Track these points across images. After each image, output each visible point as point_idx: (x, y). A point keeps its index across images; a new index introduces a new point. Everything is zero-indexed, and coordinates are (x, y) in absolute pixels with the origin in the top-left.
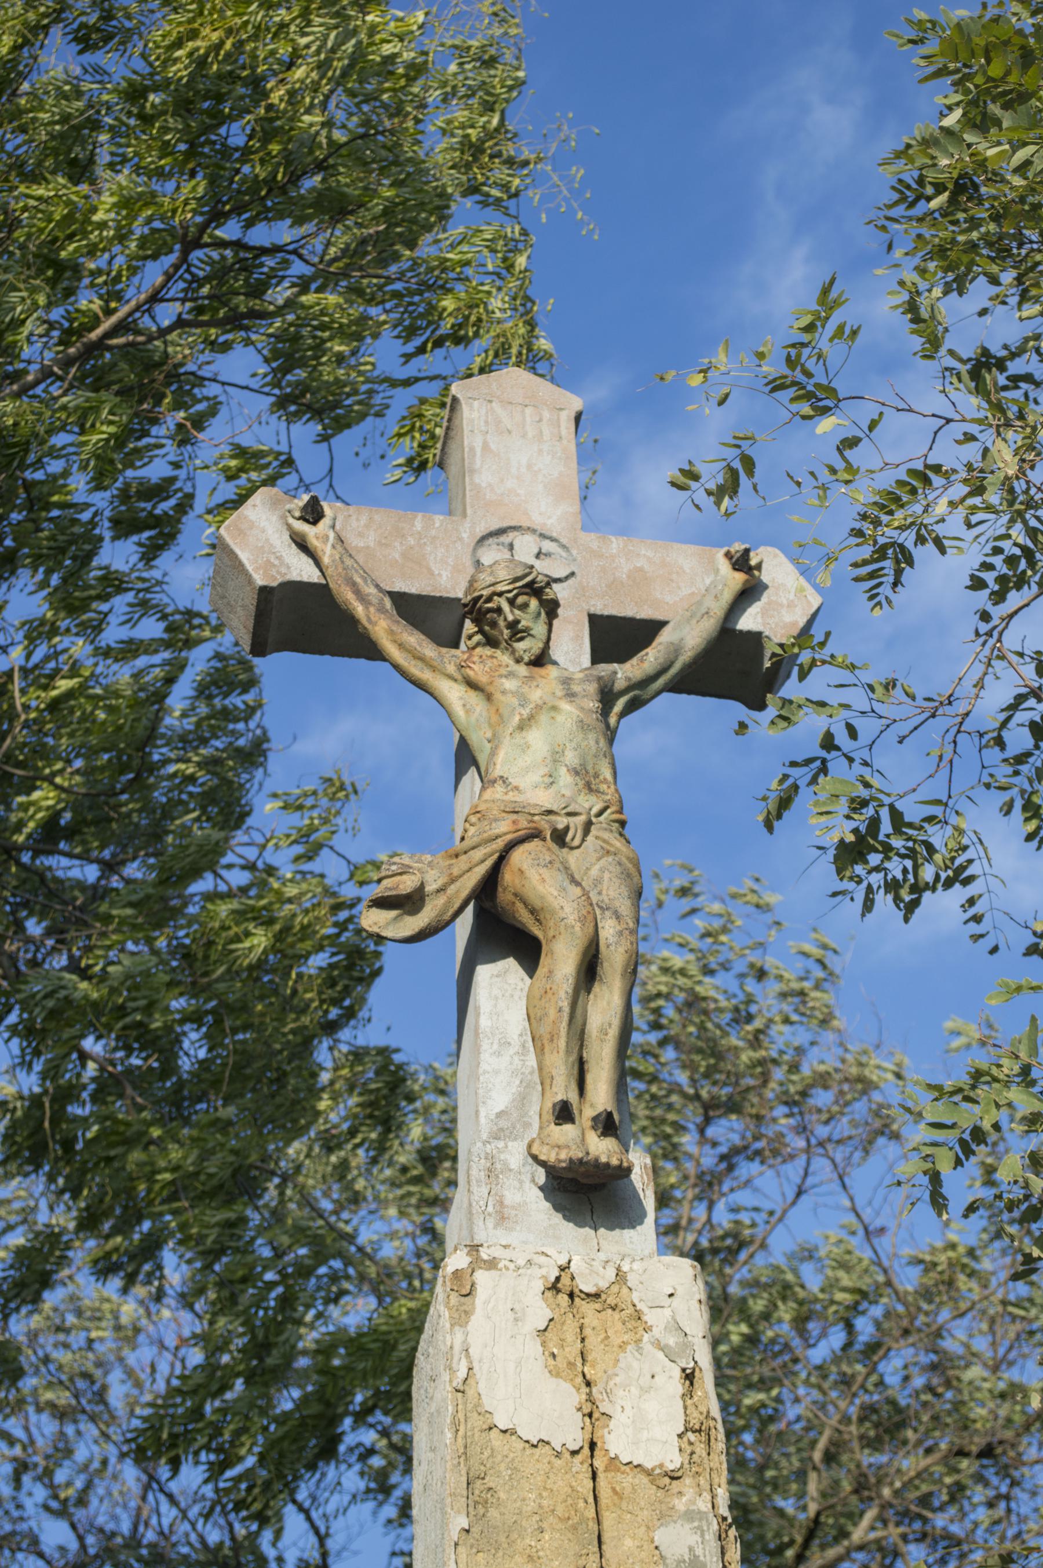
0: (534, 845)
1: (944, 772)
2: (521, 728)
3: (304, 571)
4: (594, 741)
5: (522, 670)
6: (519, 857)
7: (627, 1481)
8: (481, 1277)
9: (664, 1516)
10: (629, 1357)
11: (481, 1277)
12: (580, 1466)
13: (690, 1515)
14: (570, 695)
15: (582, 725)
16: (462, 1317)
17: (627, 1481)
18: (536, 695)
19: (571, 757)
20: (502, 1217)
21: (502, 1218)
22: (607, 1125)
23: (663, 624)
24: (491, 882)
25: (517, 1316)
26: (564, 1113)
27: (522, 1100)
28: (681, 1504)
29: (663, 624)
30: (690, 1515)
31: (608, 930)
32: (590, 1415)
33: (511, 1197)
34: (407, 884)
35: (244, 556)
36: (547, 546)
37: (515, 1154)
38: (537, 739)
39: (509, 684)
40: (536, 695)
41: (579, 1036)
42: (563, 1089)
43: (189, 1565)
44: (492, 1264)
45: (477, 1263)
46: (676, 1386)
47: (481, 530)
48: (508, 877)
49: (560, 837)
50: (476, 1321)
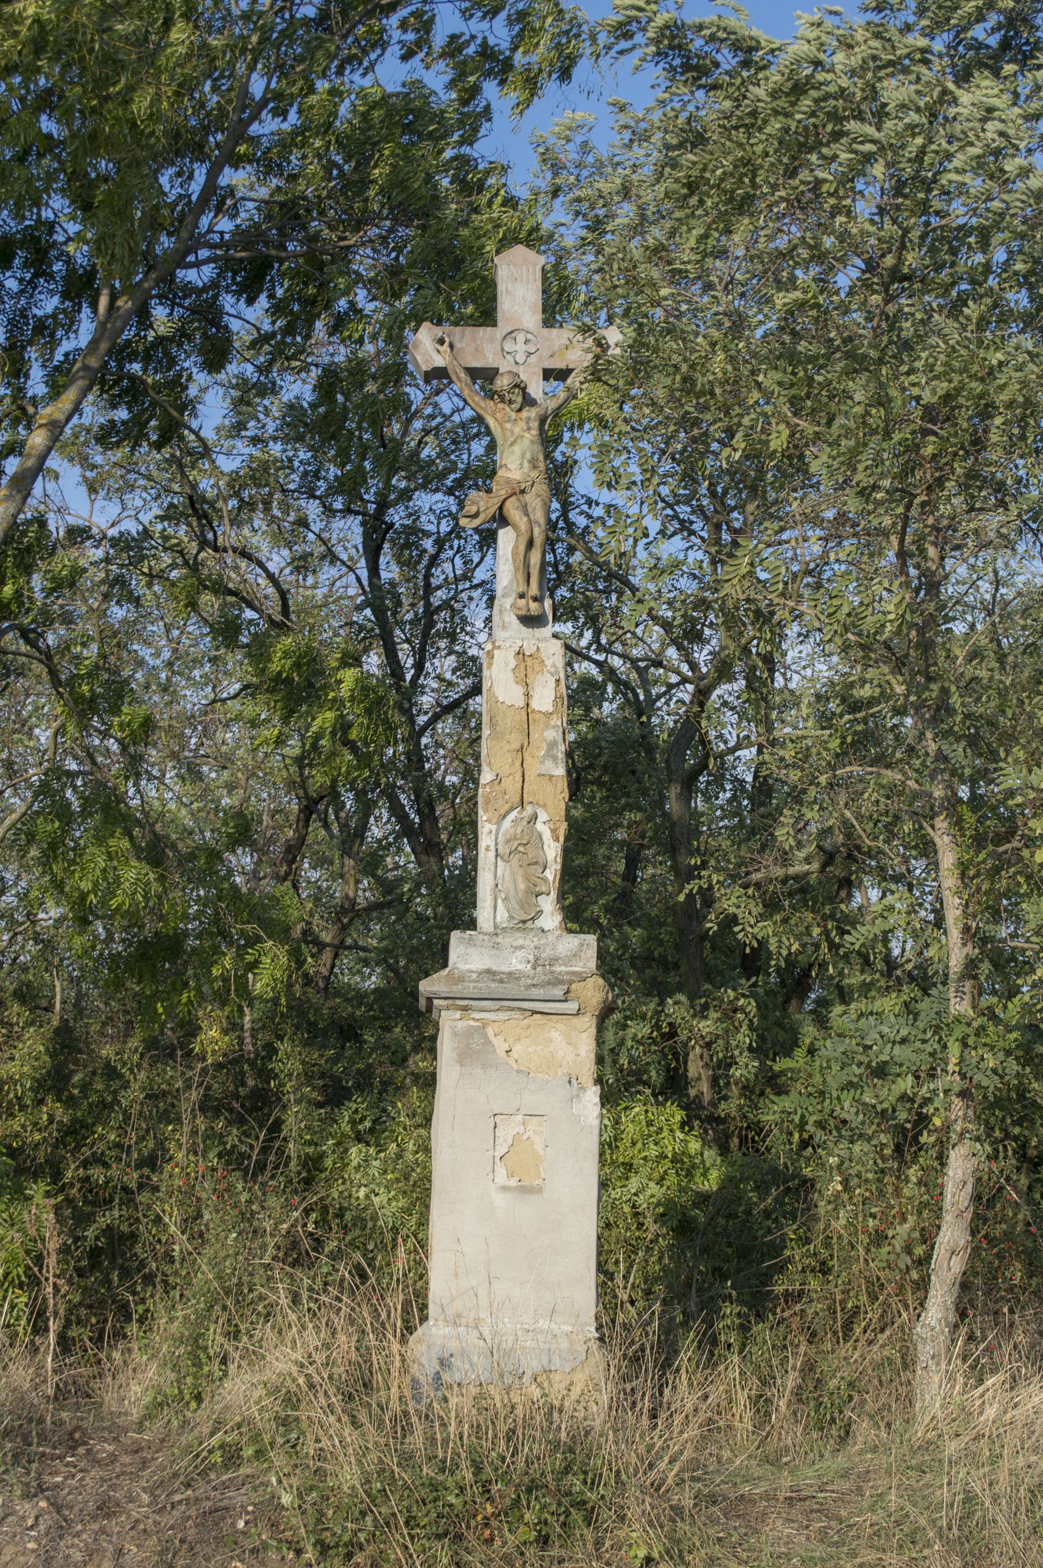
0: (513, 499)
2: (512, 444)
3: (439, 362)
4: (538, 448)
5: (513, 415)
6: (508, 503)
9: (547, 726)
18: (517, 430)
19: (528, 456)
20: (504, 627)
22: (535, 599)
24: (501, 508)
25: (506, 664)
26: (522, 596)
31: (537, 531)
32: (527, 695)
33: (507, 619)
34: (473, 509)
37: (508, 602)
38: (516, 448)
39: (508, 426)
40: (517, 430)
42: (522, 588)
45: (495, 647)
46: (552, 684)
49: (523, 492)
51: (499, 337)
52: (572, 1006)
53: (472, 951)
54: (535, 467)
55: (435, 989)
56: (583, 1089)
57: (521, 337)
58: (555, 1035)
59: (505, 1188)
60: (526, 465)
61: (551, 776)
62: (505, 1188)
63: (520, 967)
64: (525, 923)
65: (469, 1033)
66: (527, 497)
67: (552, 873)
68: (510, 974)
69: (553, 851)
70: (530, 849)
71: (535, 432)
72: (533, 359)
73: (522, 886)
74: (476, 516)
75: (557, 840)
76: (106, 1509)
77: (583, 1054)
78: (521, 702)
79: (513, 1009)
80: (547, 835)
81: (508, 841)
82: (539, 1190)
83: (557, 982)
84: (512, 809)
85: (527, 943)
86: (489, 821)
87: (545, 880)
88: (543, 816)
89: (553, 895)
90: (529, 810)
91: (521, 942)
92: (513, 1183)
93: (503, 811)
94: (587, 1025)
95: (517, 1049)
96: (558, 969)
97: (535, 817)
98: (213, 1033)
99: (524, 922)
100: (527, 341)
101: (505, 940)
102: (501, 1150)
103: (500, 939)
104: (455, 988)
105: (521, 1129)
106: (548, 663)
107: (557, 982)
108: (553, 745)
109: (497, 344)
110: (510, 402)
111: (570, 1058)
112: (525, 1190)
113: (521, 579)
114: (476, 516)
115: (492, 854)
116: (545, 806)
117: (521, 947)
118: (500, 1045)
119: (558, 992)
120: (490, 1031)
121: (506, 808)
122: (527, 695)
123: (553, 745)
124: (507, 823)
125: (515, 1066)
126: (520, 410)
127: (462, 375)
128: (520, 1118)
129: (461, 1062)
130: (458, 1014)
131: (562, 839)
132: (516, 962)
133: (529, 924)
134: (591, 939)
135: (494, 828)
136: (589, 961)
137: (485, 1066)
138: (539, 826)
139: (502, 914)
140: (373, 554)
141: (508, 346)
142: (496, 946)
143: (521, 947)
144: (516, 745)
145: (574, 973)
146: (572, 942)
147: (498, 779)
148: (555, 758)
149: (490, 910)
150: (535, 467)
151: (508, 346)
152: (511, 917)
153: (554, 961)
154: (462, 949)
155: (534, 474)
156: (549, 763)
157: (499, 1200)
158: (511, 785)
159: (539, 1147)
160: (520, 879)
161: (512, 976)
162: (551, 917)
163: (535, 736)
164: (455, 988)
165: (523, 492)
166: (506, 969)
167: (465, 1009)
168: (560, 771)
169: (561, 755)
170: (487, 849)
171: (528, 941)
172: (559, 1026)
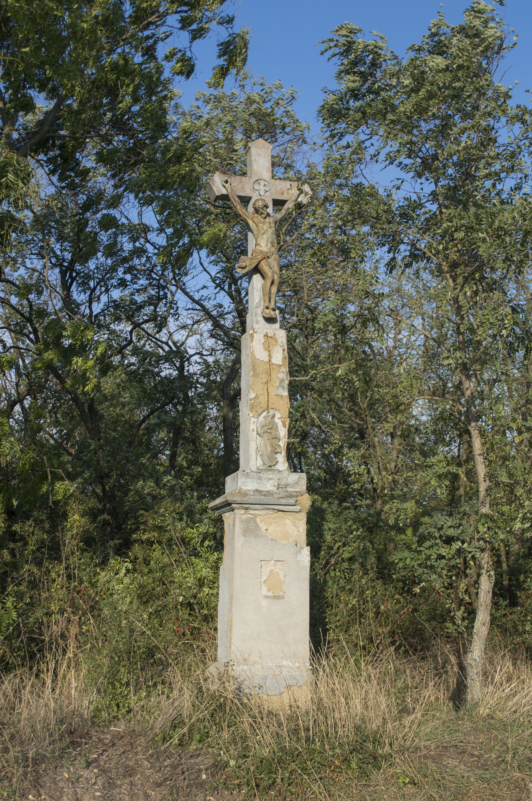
0: (264, 260)
1: (369, 137)
2: (263, 234)
3: (224, 192)
4: (274, 236)
5: (262, 220)
6: (262, 262)
7: (274, 366)
8: (255, 334)
9: (279, 372)
10: (275, 347)
11: (255, 334)
12: (268, 364)
13: (283, 372)
14: (271, 227)
15: (272, 234)
16: (252, 341)
17: (274, 366)
19: (270, 240)
21: (257, 323)
23: (286, 201)
24: (257, 265)
26: (267, 308)
27: (260, 301)
28: (282, 370)
29: (286, 201)
30: (283, 372)
31: (276, 277)
32: (270, 356)
33: (259, 319)
34: (244, 265)
35: (214, 189)
36: (266, 183)
37: (259, 311)
39: (261, 225)
40: (265, 227)
41: (270, 293)
43: (531, 466)
44: (256, 332)
46: (281, 351)
47: (254, 180)
48: (260, 265)
50: (254, 342)
51: (252, 182)
52: (297, 508)
53: (248, 480)
54: (273, 246)
55: (235, 499)
56: (302, 548)
57: (262, 183)
58: (288, 521)
59: (266, 597)
60: (269, 245)
61: (282, 396)
62: (266, 597)
63: (271, 488)
64: (271, 467)
65: (248, 521)
66: (270, 260)
67: (283, 444)
68: (268, 492)
69: (283, 432)
70: (273, 431)
71: (274, 229)
72: (268, 194)
73: (269, 449)
74: (244, 268)
75: (285, 427)
76: (130, 772)
77: (301, 531)
78: (267, 360)
79: (268, 509)
80: (280, 424)
81: (263, 427)
82: (282, 597)
83: (291, 496)
84: (264, 411)
85: (274, 477)
86: (253, 417)
87: (279, 446)
88: (278, 415)
89: (284, 453)
90: (272, 412)
91: (271, 476)
92: (270, 594)
93: (260, 412)
94: (303, 518)
95: (271, 528)
96: (289, 489)
97: (274, 416)
98: (76, 517)
99: (270, 466)
100: (265, 185)
101: (264, 475)
102: (264, 579)
103: (261, 475)
104: (244, 499)
105: (273, 568)
106: (279, 341)
107: (291, 496)
108: (282, 381)
109: (251, 185)
110: (262, 213)
111: (296, 533)
112: (276, 597)
113: (267, 299)
114: (244, 268)
115: (255, 433)
116: (279, 410)
117: (271, 479)
118: (263, 526)
119: (292, 501)
120: (258, 520)
121: (261, 410)
122: (270, 356)
123: (282, 381)
124: (261, 418)
125: (270, 537)
126: (265, 218)
127: (237, 199)
128: (273, 562)
129: (244, 535)
130: (243, 511)
131: (287, 426)
132: (269, 486)
133: (273, 468)
134: (304, 475)
135: (256, 420)
136: (303, 485)
137: (256, 537)
138: (276, 420)
139: (260, 463)
140: (66, 287)
141: (256, 187)
142: (260, 478)
143: (271, 479)
144: (265, 380)
145: (297, 492)
146: (294, 477)
147: (256, 397)
148: (283, 387)
149: (254, 460)
150: (273, 246)
151: (256, 187)
152: (264, 464)
153: (287, 486)
154: (243, 479)
155: (273, 249)
156: (281, 390)
157: (264, 603)
158: (263, 399)
159: (281, 576)
160: (268, 446)
161: (268, 493)
162: (282, 464)
163: (274, 376)
164: (244, 499)
165: (268, 257)
166: (266, 490)
167: (247, 509)
168: (286, 393)
169: (286, 386)
170: (253, 430)
171: (274, 476)
172: (289, 517)
